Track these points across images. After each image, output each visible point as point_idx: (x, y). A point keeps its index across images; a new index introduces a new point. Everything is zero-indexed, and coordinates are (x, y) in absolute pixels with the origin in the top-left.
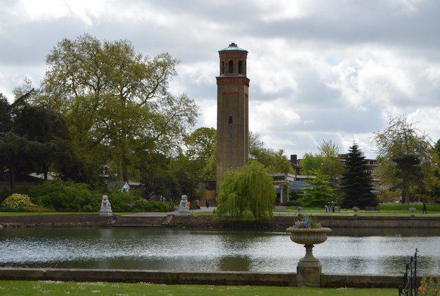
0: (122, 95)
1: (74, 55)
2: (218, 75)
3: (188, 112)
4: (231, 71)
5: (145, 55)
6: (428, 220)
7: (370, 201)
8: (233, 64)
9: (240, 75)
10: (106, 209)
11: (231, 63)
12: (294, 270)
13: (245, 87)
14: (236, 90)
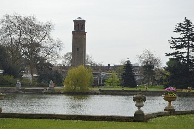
0: (31, 38)
1: (10, 21)
2: (73, 30)
3: (59, 46)
4: (78, 29)
5: (41, 20)
6: (153, 92)
7: (134, 85)
8: (79, 27)
9: (82, 30)
10: (19, 85)
11: (78, 25)
12: (133, 115)
13: (84, 35)
14: (80, 37)
